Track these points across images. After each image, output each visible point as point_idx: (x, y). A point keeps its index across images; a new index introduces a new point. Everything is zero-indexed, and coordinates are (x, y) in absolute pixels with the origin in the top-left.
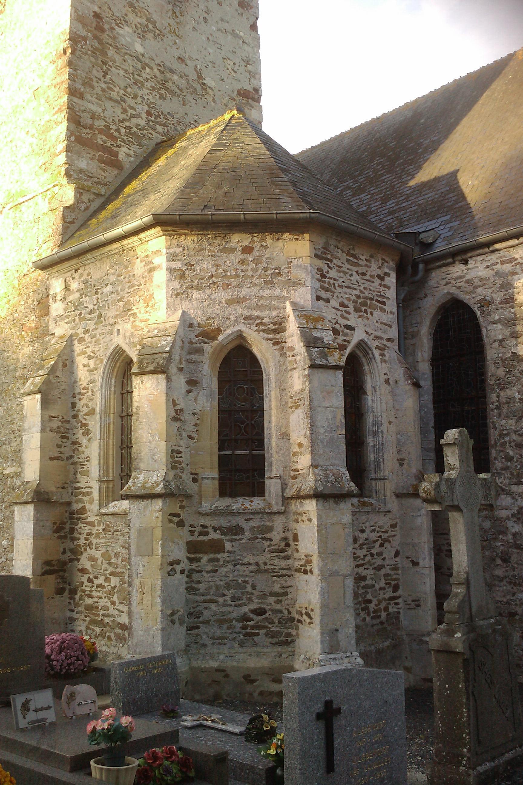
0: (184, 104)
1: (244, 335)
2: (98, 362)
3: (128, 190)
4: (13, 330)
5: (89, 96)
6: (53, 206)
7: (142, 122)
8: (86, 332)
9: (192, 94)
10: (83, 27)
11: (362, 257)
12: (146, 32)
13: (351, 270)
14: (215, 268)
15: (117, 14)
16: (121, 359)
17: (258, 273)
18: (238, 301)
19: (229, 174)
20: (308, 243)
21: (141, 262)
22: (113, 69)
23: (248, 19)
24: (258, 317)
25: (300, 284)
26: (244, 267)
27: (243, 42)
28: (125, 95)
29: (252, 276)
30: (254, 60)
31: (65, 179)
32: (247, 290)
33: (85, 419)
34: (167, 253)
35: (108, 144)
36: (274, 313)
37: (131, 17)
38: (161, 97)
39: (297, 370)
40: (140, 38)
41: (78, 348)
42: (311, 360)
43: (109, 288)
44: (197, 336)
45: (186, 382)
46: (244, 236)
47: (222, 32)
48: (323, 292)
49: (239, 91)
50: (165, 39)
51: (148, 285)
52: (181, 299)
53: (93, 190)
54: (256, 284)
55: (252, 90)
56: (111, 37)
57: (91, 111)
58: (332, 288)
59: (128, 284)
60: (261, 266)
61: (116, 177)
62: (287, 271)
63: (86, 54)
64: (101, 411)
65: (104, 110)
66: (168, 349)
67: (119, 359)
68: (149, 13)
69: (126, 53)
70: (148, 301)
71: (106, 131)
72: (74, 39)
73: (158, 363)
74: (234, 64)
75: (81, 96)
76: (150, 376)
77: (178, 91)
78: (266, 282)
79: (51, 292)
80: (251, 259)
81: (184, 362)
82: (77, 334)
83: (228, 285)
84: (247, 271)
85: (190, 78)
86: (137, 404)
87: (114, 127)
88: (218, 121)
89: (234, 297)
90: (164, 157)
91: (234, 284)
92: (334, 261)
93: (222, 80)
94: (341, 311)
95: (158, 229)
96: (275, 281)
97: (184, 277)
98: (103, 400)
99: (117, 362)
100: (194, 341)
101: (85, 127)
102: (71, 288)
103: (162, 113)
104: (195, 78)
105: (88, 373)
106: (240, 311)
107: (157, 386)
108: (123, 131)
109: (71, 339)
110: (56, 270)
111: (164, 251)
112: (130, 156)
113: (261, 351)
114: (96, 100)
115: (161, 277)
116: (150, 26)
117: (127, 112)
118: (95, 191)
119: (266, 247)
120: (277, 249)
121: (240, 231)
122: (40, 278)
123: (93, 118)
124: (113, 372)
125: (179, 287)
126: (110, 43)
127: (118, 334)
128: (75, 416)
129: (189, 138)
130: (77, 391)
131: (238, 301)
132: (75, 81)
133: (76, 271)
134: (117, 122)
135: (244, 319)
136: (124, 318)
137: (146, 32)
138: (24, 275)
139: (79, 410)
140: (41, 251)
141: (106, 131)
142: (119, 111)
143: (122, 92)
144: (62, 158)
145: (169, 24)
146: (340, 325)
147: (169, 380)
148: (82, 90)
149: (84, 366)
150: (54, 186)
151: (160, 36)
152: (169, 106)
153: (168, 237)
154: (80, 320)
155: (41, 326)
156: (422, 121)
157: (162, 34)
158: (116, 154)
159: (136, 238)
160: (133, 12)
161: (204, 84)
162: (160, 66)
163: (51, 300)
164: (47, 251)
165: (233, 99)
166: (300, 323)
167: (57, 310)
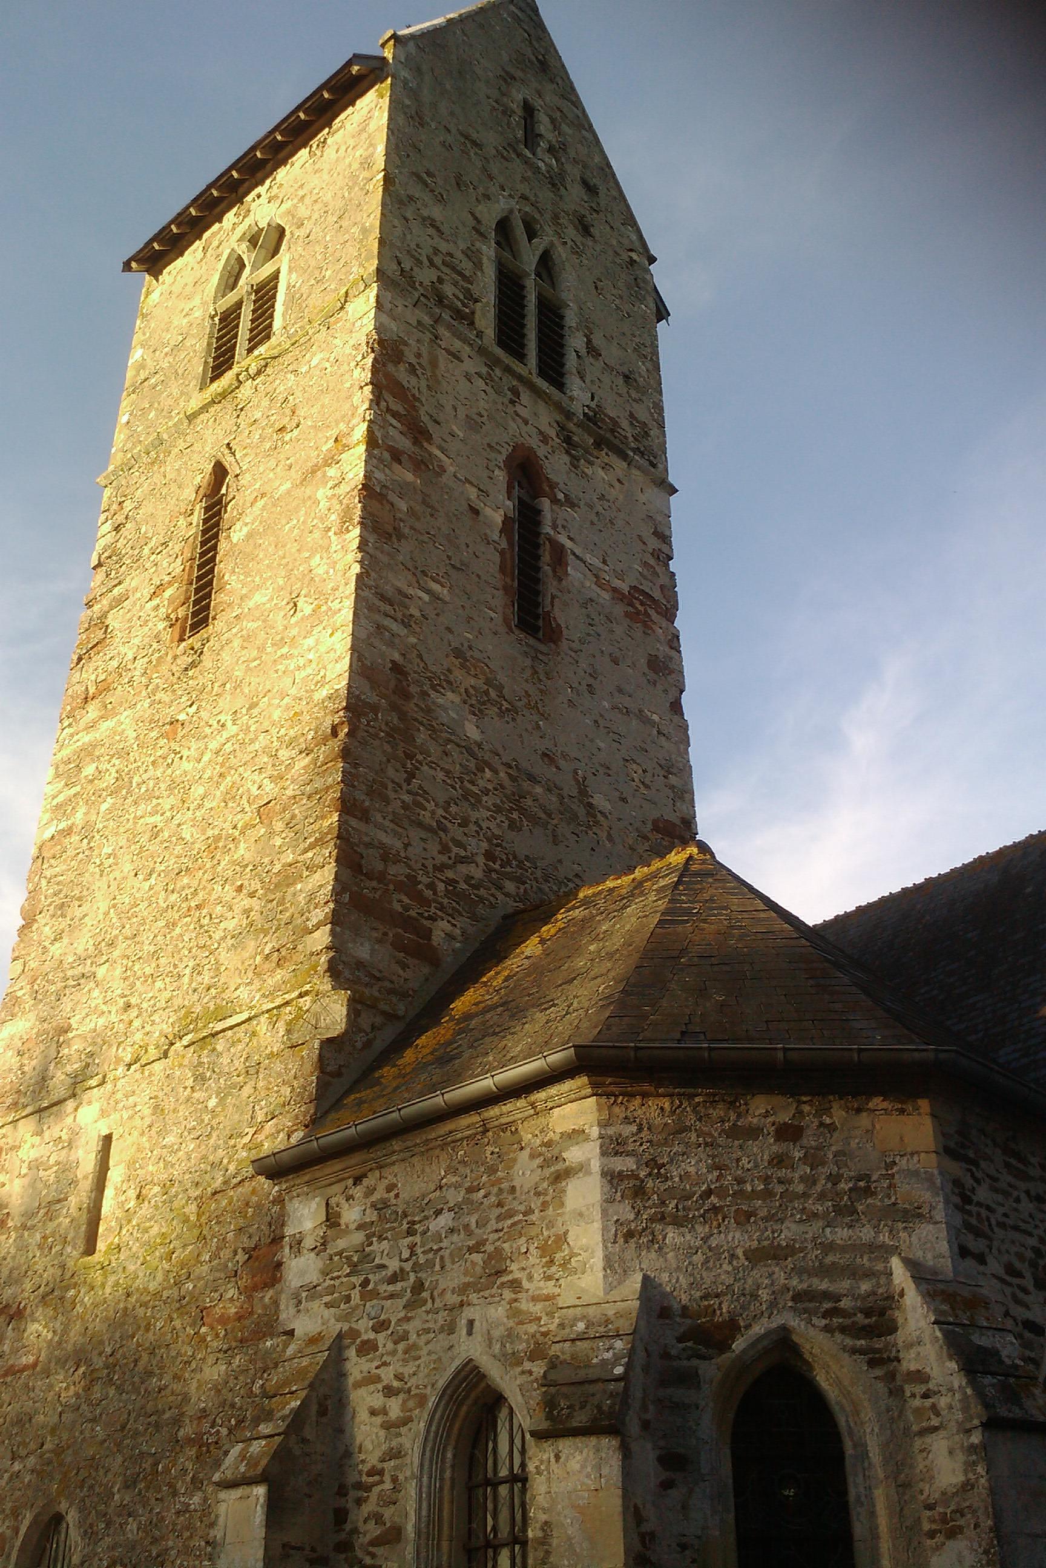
0: (556, 841)
1: (795, 1338)
2: (411, 1404)
3: (461, 1005)
4: (177, 1323)
5: (378, 817)
6: (296, 1037)
7: (477, 873)
8: (381, 1326)
9: (569, 824)
10: (372, 688)
11: (1033, 1160)
12: (484, 703)
13: (1015, 1188)
14: (716, 1173)
15: (434, 669)
16: (473, 1396)
17: (819, 1188)
18: (773, 1253)
19: (716, 969)
20: (928, 1121)
21: (532, 1156)
22: (425, 768)
23: (665, 691)
24: (826, 1295)
25: (920, 1216)
26: (782, 1173)
27: (659, 733)
28: (444, 817)
29: (805, 1195)
30: (681, 766)
31: (327, 979)
32: (793, 1226)
33: (373, 1556)
34: (601, 1137)
35: (413, 913)
36: (865, 1287)
37: (458, 675)
38: (513, 826)
39: (942, 1433)
40: (475, 715)
41: (356, 1366)
42: (987, 1406)
43: (445, 1220)
44: (680, 1340)
45: (661, 1460)
46: (778, 1100)
47: (621, 711)
48: (971, 1237)
49: (655, 822)
50: (519, 718)
51: (550, 1211)
52: (639, 1247)
53: (382, 1006)
54: (815, 1215)
55: (678, 822)
56: (422, 709)
57: (382, 846)
58: (986, 1229)
59: (497, 1211)
60: (824, 1171)
61: (427, 979)
62: (885, 1184)
63: (375, 736)
64: (418, 1533)
65: (406, 846)
66: (619, 1370)
67: (466, 1397)
68: (492, 671)
69: (450, 741)
70: (553, 1249)
71: (409, 886)
72: (355, 706)
73: (599, 1407)
74: (644, 771)
75: (365, 816)
76: (579, 1441)
77: (543, 816)
78: (839, 1210)
79: (289, 1231)
80: (797, 1155)
81: (651, 1407)
82: (354, 1334)
83: (749, 1215)
84: (790, 1181)
85: (565, 793)
86: (543, 1517)
87: (425, 880)
88: (653, 868)
89: (766, 1243)
90: (534, 940)
91: (763, 1213)
92: (983, 1164)
93: (624, 800)
94: (1010, 1285)
95: (583, 1080)
96: (860, 1208)
97: (641, 1195)
98: (425, 1505)
99: (461, 1404)
100: (673, 1352)
101: (369, 876)
102: (342, 1221)
103: (515, 858)
104: (575, 793)
105: (382, 1433)
106: (781, 1277)
107: (598, 1467)
108: (441, 886)
109: (338, 1345)
110: (307, 1178)
111: (595, 1132)
112: (454, 939)
113: (838, 1382)
114: (392, 825)
115: (585, 1194)
116: (493, 694)
117: (450, 851)
118: (387, 1008)
119: (832, 1128)
120: (858, 1132)
121: (770, 1091)
122: (255, 1199)
123: (385, 858)
124: (451, 1427)
125: (632, 1216)
126: (420, 719)
127: (470, 1333)
128: (345, 1547)
129: (587, 902)
130: (352, 1478)
131: (773, 1253)
132: (354, 786)
133: (357, 1180)
134: (430, 869)
135: (793, 1299)
136: (486, 1293)
137: (484, 703)
138: (215, 1193)
139: (355, 1531)
140: (260, 1137)
141: (409, 886)
142: (434, 848)
143: (440, 812)
144: (322, 938)
145: (526, 692)
146: (1015, 1320)
147: (626, 1451)
148: (367, 804)
149: (373, 1413)
150: (301, 996)
151: (510, 712)
152: (526, 843)
153: (604, 1099)
154: (363, 1297)
155: (251, 1313)
156: (1029, 890)
157: (514, 710)
158: (428, 934)
159: (521, 1103)
160: (463, 666)
161: (590, 805)
162: (511, 767)
163: (287, 1250)
164: (276, 1137)
165: (645, 838)
166: (936, 1311)
167: (302, 1273)
